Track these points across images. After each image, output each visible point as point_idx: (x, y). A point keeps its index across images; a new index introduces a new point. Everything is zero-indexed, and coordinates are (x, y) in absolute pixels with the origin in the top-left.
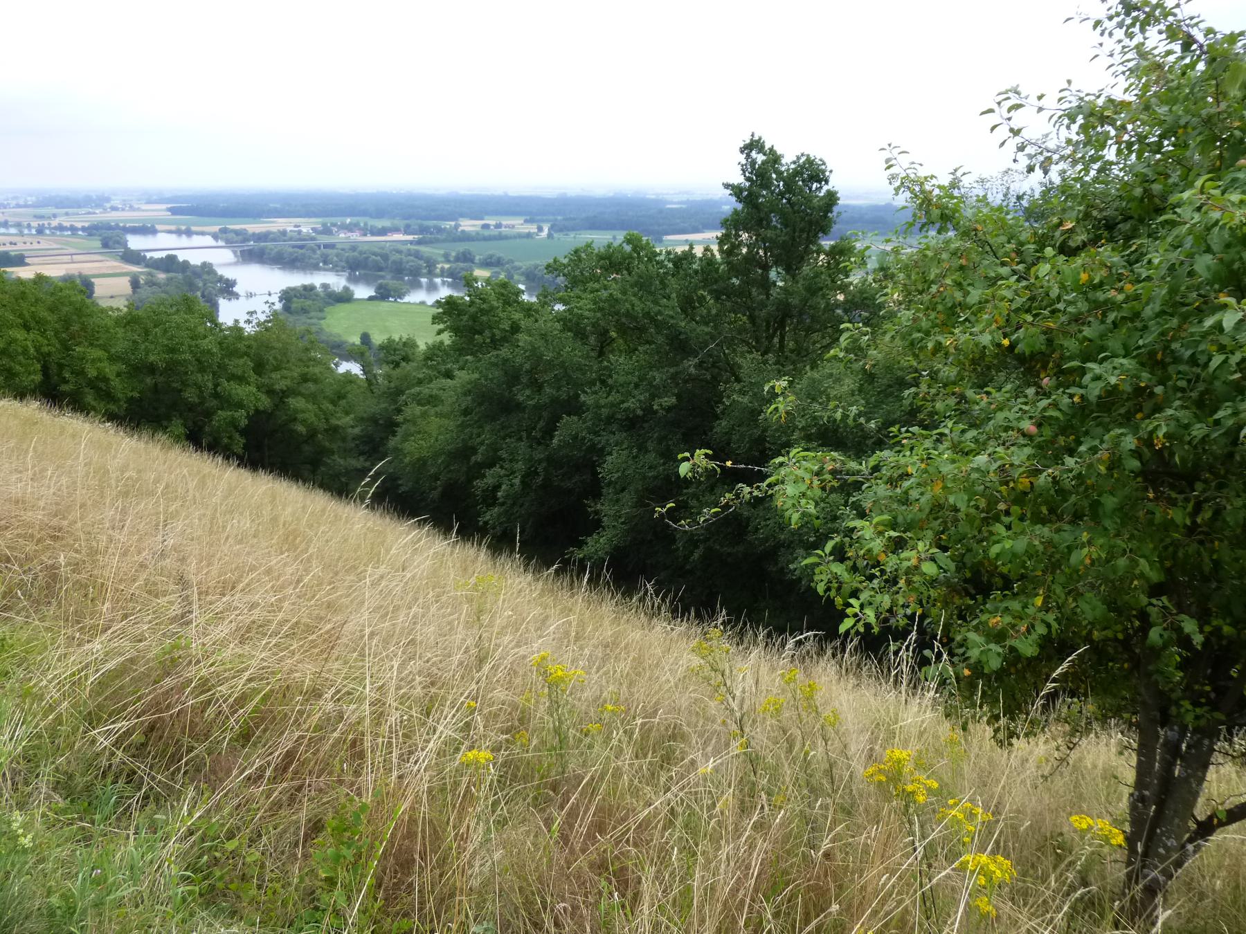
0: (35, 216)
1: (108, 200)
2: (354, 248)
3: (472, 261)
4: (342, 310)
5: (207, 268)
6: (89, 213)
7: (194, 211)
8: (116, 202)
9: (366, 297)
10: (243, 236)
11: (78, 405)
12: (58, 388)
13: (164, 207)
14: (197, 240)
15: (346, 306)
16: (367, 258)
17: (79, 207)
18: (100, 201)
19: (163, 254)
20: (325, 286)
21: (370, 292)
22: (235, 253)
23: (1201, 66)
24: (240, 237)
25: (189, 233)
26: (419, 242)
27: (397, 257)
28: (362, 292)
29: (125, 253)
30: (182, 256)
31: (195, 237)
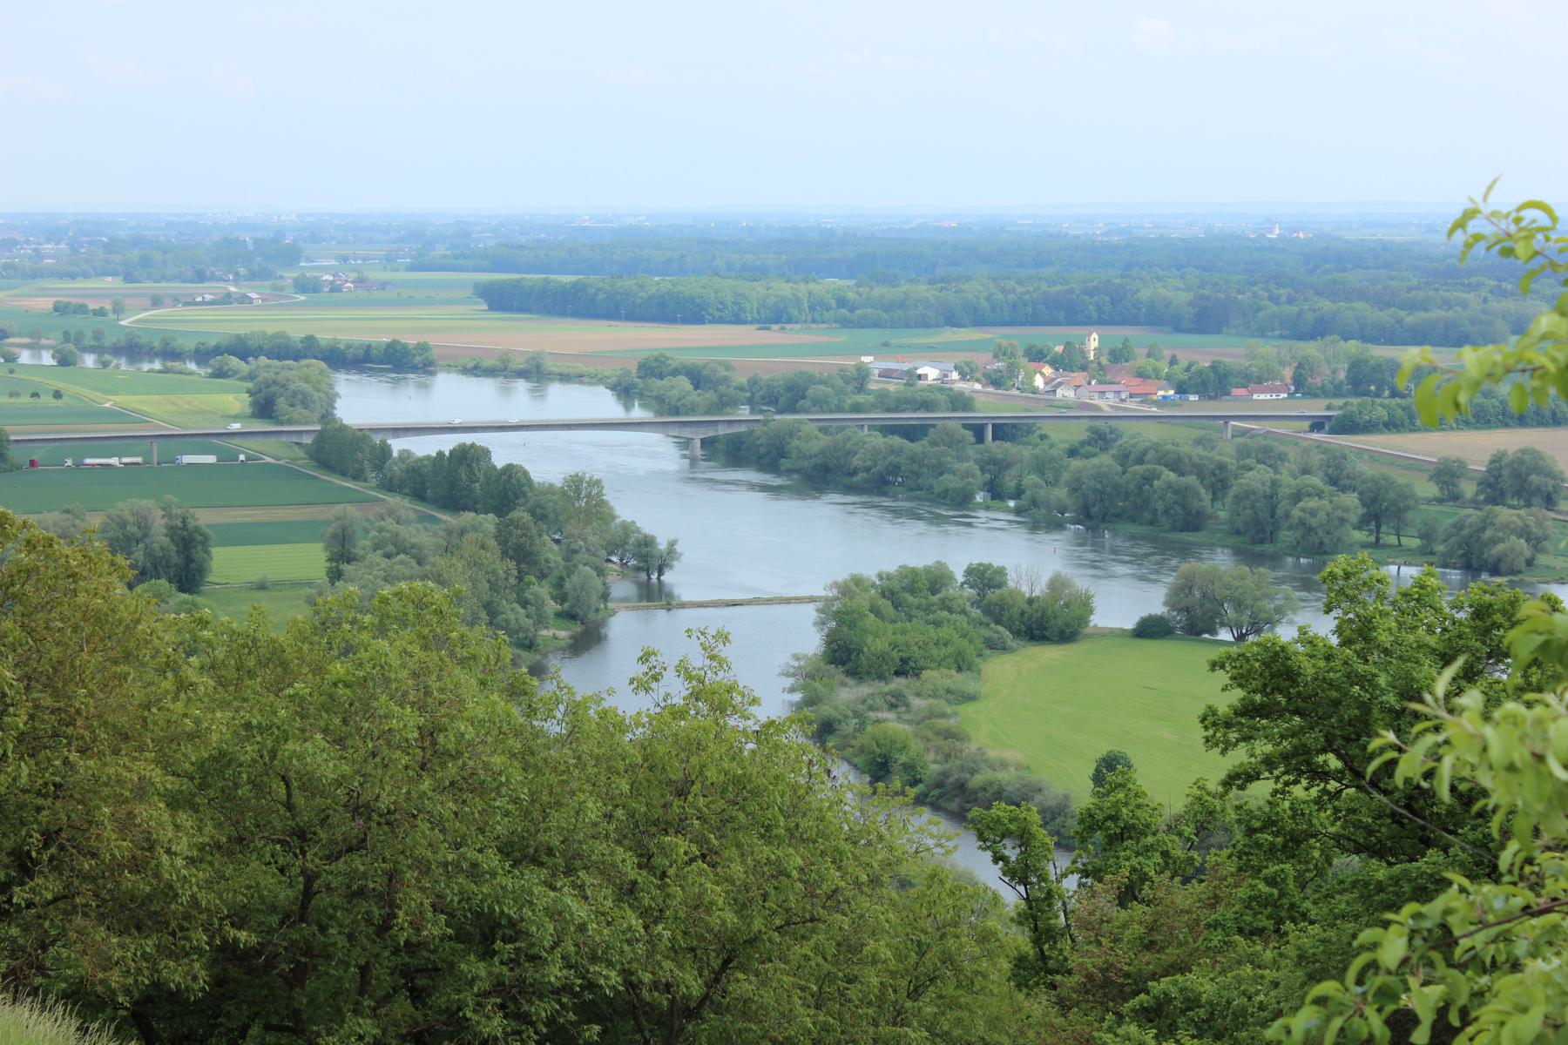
1: (290, 255)
2: (1100, 439)
4: (1016, 672)
5: (581, 502)
6: (226, 300)
7: (552, 286)
8: (323, 267)
9: (1130, 624)
14: (565, 401)
16: (1148, 479)
17: (200, 277)
18: (263, 256)
19: (446, 444)
20: (985, 579)
21: (1153, 601)
22: (685, 444)
24: (711, 396)
25: (536, 373)
26: (1348, 425)
27: (1257, 478)
28: (1122, 599)
29: (321, 438)
30: (503, 452)
31: (555, 390)
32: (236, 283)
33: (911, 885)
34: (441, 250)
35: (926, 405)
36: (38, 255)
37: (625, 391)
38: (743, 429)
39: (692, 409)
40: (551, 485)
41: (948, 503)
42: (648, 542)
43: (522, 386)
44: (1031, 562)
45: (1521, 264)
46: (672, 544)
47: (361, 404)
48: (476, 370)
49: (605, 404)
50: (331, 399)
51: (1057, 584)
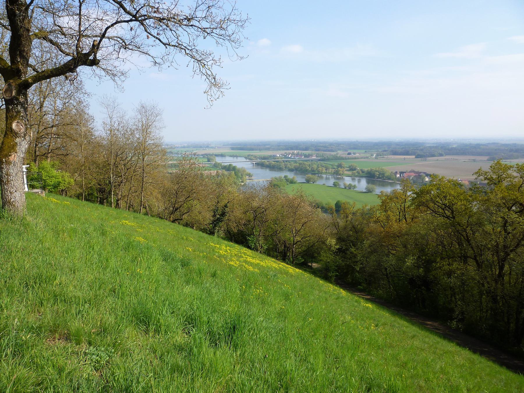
14: (240, 159)
19: (228, 164)
25: (237, 156)
30: (234, 164)
37: (246, 158)
40: (457, 185)
41: (280, 169)
43: (235, 158)
44: (291, 176)
45: (496, 154)
47: (218, 160)
48: (231, 156)
49: (244, 160)
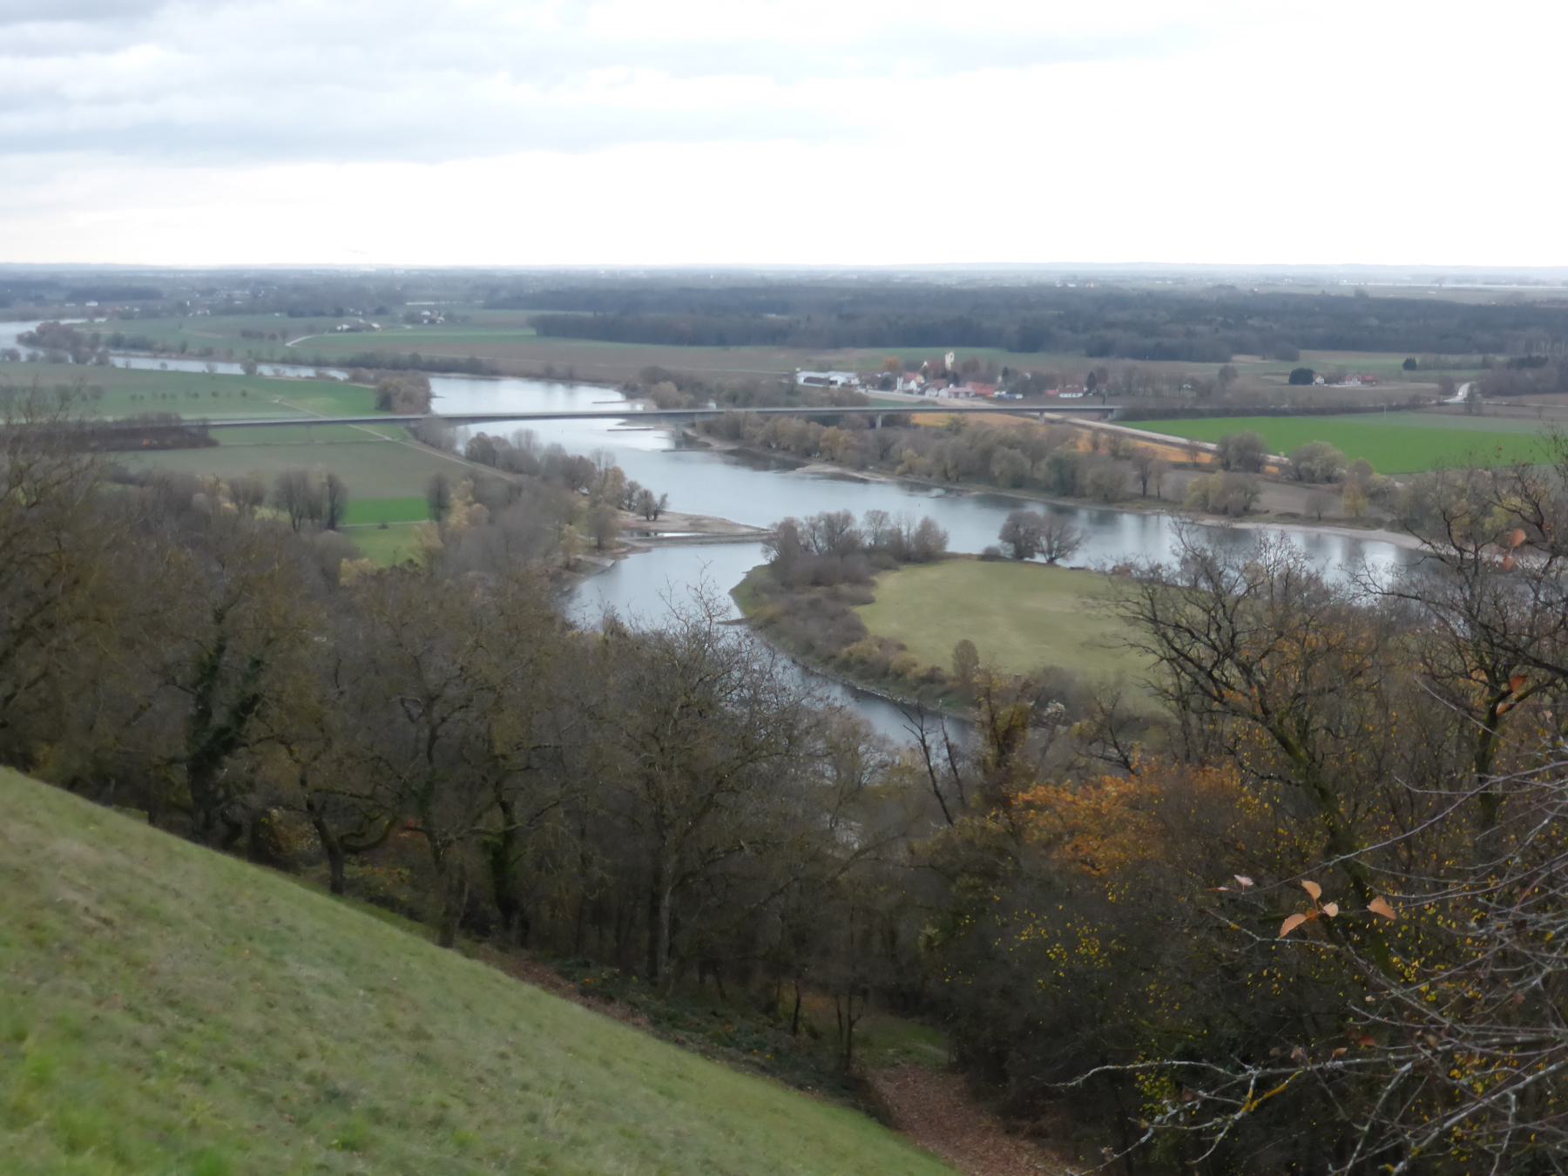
0: (246, 334)
3: (1256, 465)
9: (977, 549)
10: (696, 388)
11: (227, 844)
12: (199, 788)
13: (523, 315)
14: (587, 398)
15: (930, 574)
20: (877, 517)
23: (1518, 860)
32: (363, 316)
33: (403, 401)
34: (504, 294)
35: (838, 402)
36: (230, 299)
38: (712, 418)
39: (678, 405)
42: (646, 495)
46: (664, 497)
50: (429, 396)
51: (927, 526)
